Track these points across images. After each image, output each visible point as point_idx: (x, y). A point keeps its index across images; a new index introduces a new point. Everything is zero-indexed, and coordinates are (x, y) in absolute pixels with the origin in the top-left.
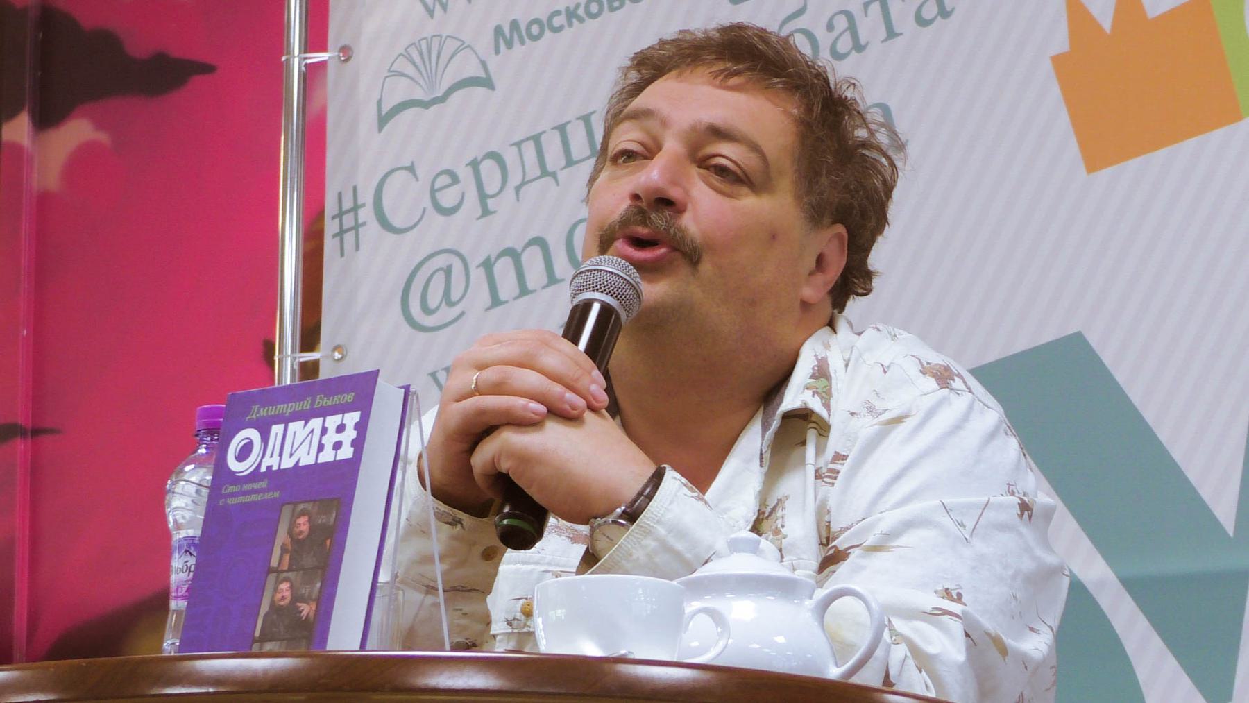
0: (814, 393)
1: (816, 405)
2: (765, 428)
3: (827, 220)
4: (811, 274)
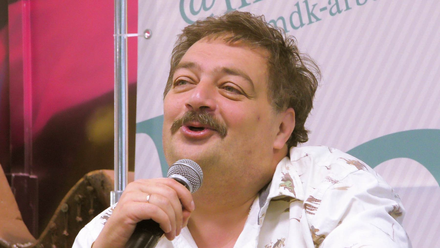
0: (285, 188)
1: (287, 193)
2: (261, 205)
3: (285, 107)
4: (278, 134)
